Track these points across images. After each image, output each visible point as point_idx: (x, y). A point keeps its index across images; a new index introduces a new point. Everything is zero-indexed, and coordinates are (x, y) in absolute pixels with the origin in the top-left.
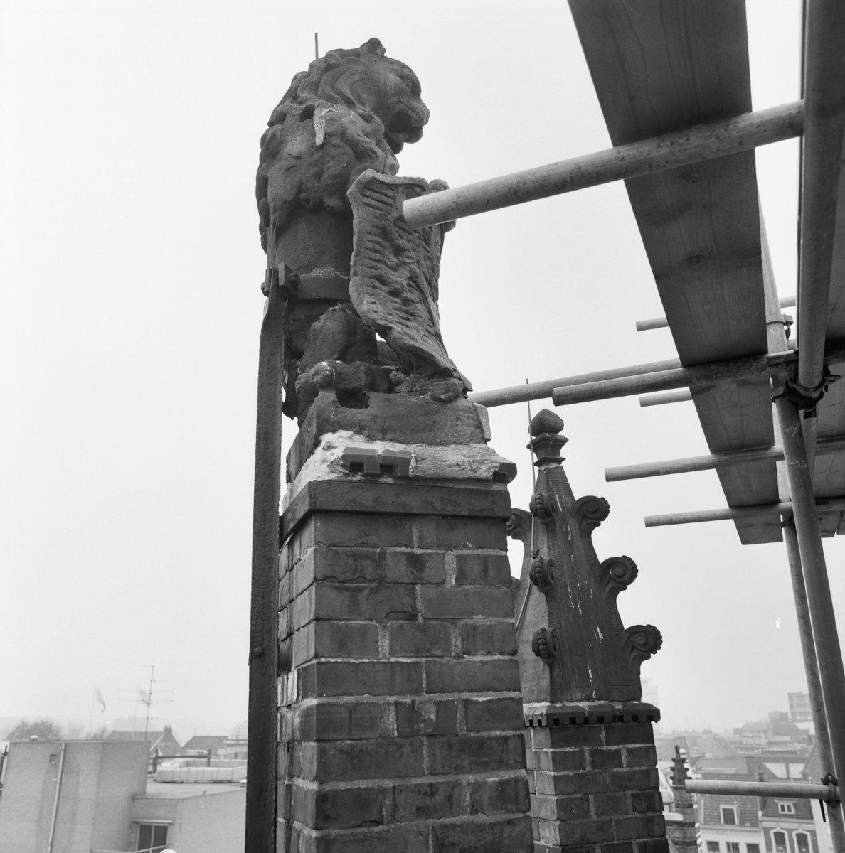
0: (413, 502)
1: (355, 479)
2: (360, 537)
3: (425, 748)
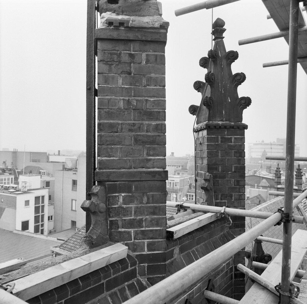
0: (131, 36)
1: (111, 28)
2: (113, 47)
3: (132, 113)
